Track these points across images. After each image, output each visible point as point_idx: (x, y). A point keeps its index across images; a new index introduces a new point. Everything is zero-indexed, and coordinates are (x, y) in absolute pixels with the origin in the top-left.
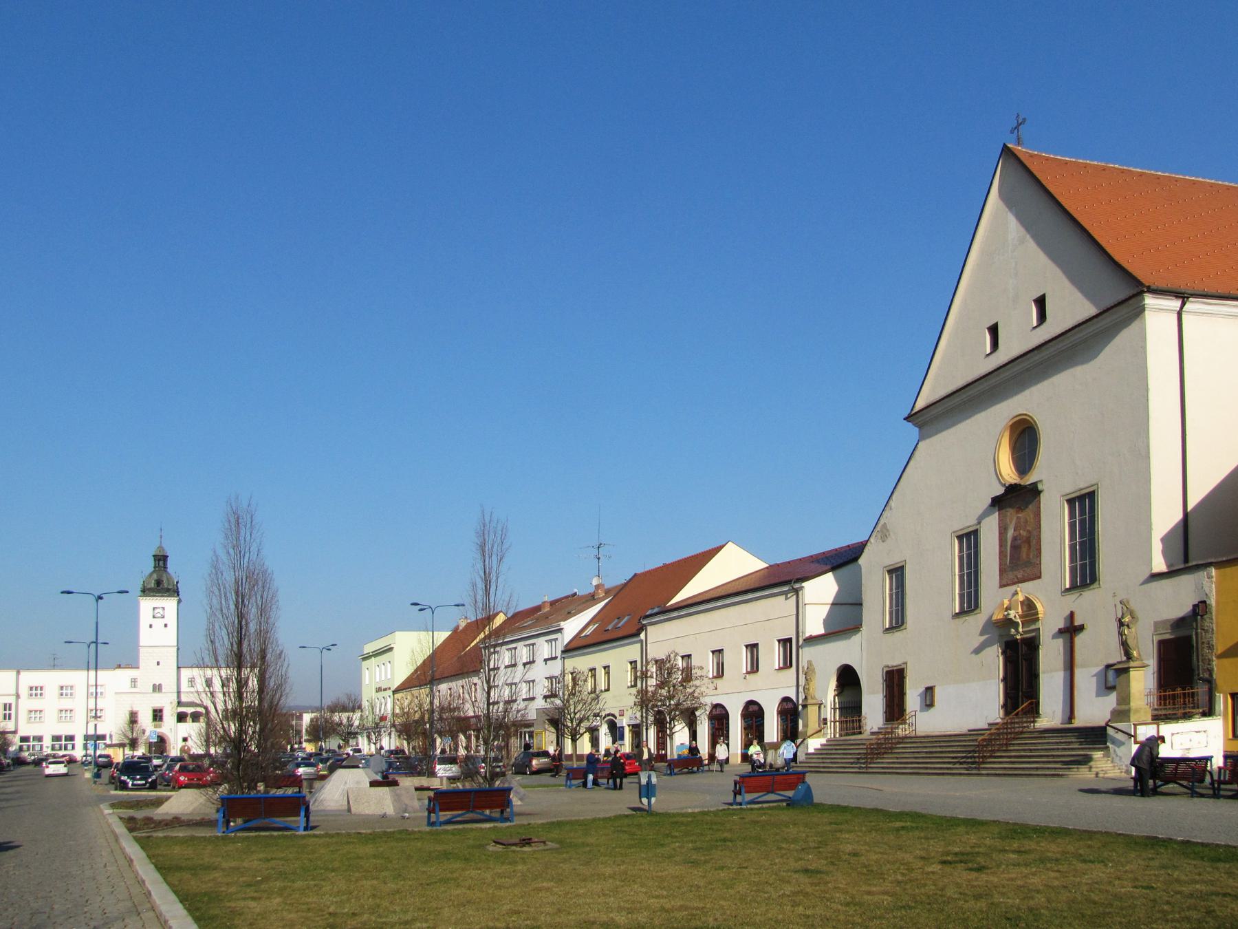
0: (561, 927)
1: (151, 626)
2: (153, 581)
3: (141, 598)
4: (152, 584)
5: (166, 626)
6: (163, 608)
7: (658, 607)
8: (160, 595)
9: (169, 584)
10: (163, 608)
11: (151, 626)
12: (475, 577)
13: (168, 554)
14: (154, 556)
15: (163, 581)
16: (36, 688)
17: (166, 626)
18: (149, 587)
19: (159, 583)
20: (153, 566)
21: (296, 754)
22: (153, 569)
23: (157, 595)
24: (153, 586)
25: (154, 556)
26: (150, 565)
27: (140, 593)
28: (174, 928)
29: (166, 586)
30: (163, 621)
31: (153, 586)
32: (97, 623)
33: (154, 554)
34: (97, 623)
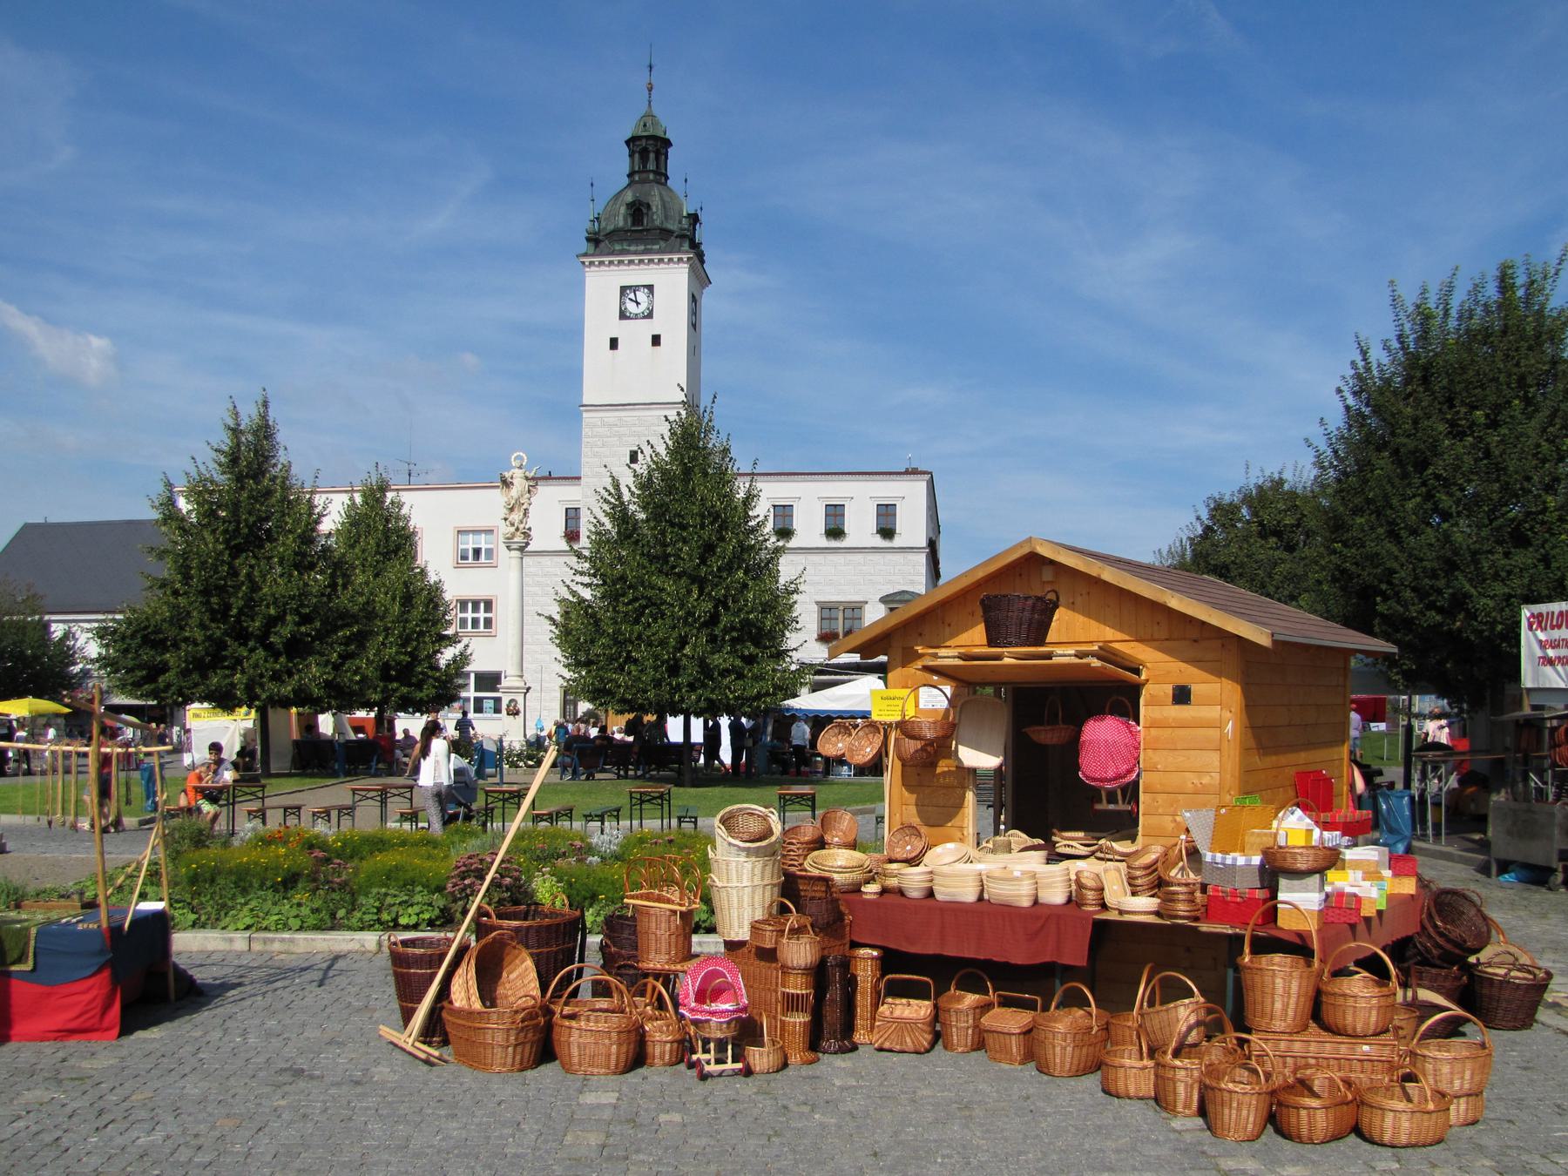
1: (614, 343)
2: (623, 210)
3: (587, 260)
4: (621, 220)
5: (656, 340)
6: (650, 288)
8: (642, 248)
9: (666, 217)
10: (650, 288)
11: (614, 343)
15: (649, 207)
16: (476, 605)
17: (656, 340)
18: (611, 227)
19: (638, 210)
22: (626, 181)
23: (633, 248)
26: (616, 168)
27: (584, 246)
29: (658, 223)
30: (646, 329)
31: (621, 224)
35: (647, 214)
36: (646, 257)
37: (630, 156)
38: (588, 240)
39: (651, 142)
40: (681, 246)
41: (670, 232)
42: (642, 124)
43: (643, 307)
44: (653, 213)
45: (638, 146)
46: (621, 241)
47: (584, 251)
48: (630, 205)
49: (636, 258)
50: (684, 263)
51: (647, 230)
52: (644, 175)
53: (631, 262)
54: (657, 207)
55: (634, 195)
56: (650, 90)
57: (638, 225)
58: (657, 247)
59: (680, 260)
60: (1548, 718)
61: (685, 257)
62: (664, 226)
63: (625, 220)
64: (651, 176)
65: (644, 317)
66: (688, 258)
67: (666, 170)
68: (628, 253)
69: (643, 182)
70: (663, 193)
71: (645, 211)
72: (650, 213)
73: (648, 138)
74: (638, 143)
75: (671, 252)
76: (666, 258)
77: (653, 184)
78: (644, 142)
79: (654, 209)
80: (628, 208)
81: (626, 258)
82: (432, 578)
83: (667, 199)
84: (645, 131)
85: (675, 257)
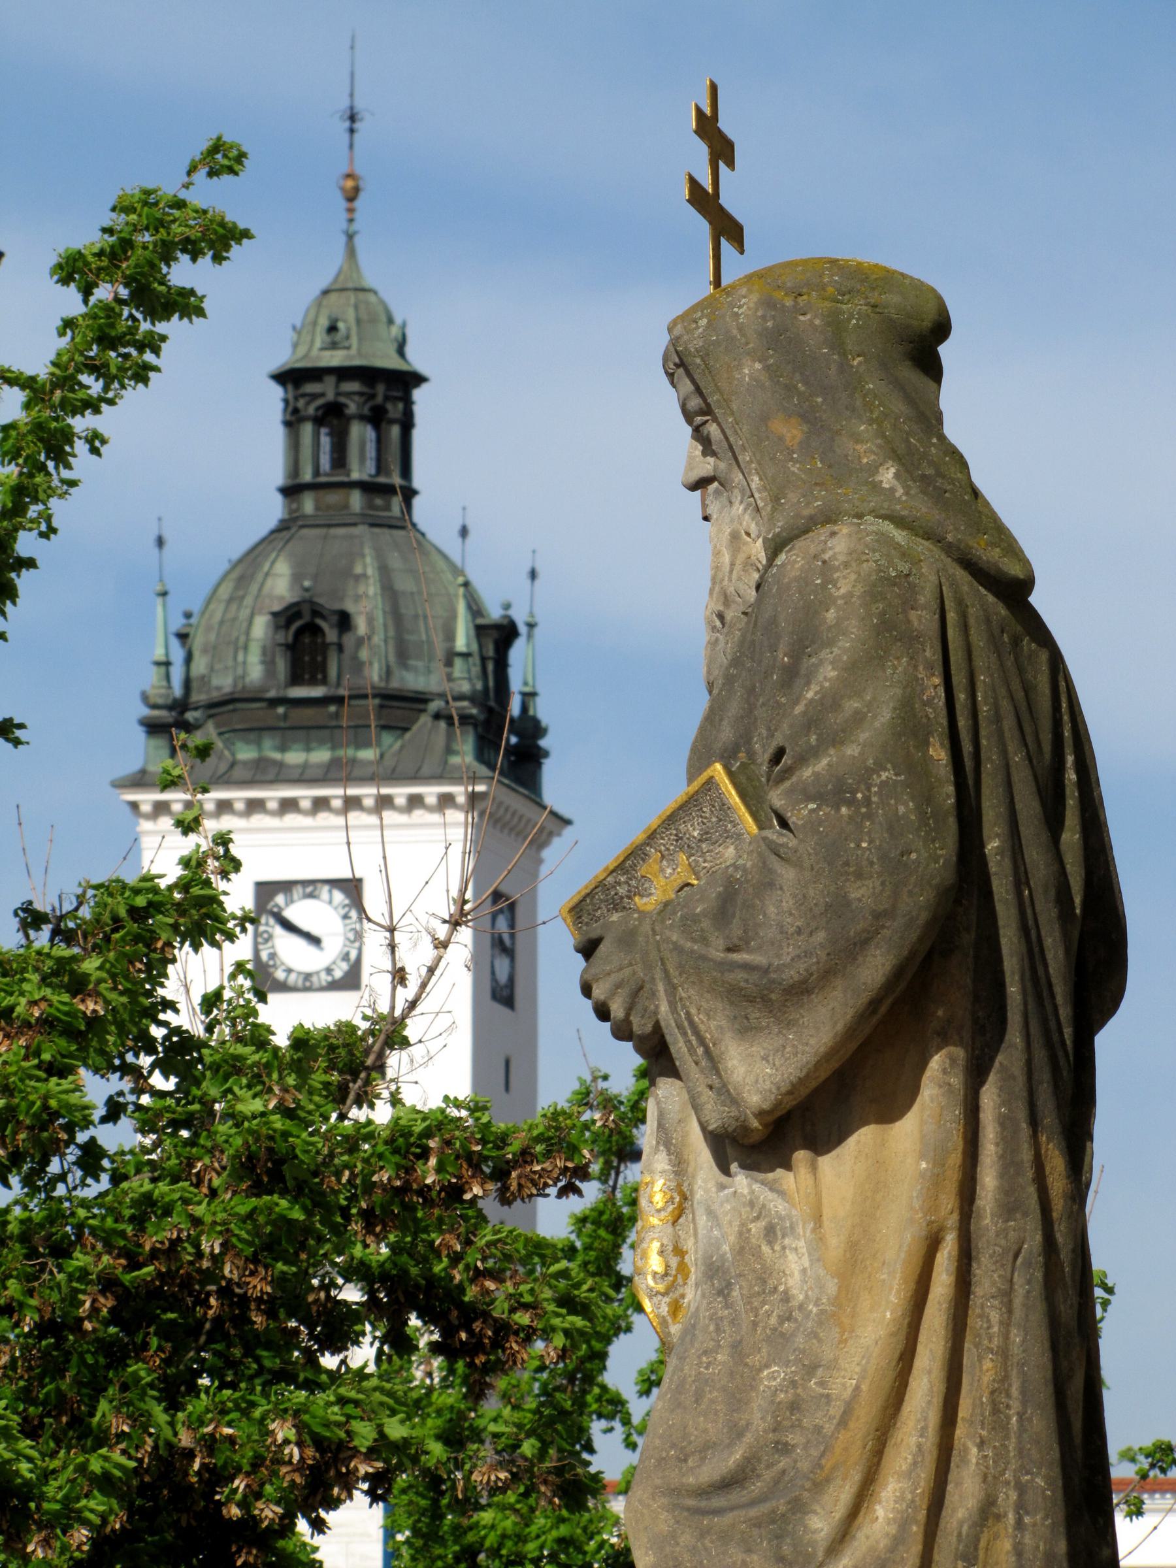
0: (469, 1554)
2: (261, 627)
3: (147, 798)
7: (927, 744)
9: (403, 654)
12: (858, 719)
13: (417, 359)
14: (284, 377)
15: (344, 621)
18: (224, 683)
20: (277, 476)
21: (512, 1338)
22: (274, 509)
23: (294, 757)
24: (255, 672)
25: (284, 377)
28: (643, 1560)
29: (374, 675)
31: (255, 672)
32: (352, 75)
33: (283, 357)
34: (352, 75)
35: (340, 648)
36: (334, 793)
37: (288, 424)
38: (153, 728)
39: (354, 386)
40: (449, 751)
41: (418, 700)
42: (324, 322)
43: (334, 946)
44: (360, 642)
45: (314, 397)
46: (255, 732)
47: (133, 765)
48: (286, 617)
49: (304, 794)
50: (455, 806)
51: (339, 700)
52: (333, 497)
53: (289, 806)
54: (370, 621)
55: (297, 578)
56: (352, 196)
57: (313, 682)
58: (368, 754)
59: (446, 801)
60: (57, 1501)
61: (459, 792)
62: (395, 684)
63: (269, 663)
64: (356, 500)
65: (335, 986)
66: (473, 798)
67: (406, 470)
68: (276, 774)
69: (327, 521)
70: (395, 561)
71: (331, 635)
72: (348, 640)
73: (343, 373)
74: (311, 388)
75: (415, 777)
76: (400, 793)
77: (360, 530)
78: (328, 389)
79: (361, 626)
80: (277, 628)
81: (273, 795)
82: (543, 743)
83: (404, 584)
84: (334, 346)
85: (431, 792)
